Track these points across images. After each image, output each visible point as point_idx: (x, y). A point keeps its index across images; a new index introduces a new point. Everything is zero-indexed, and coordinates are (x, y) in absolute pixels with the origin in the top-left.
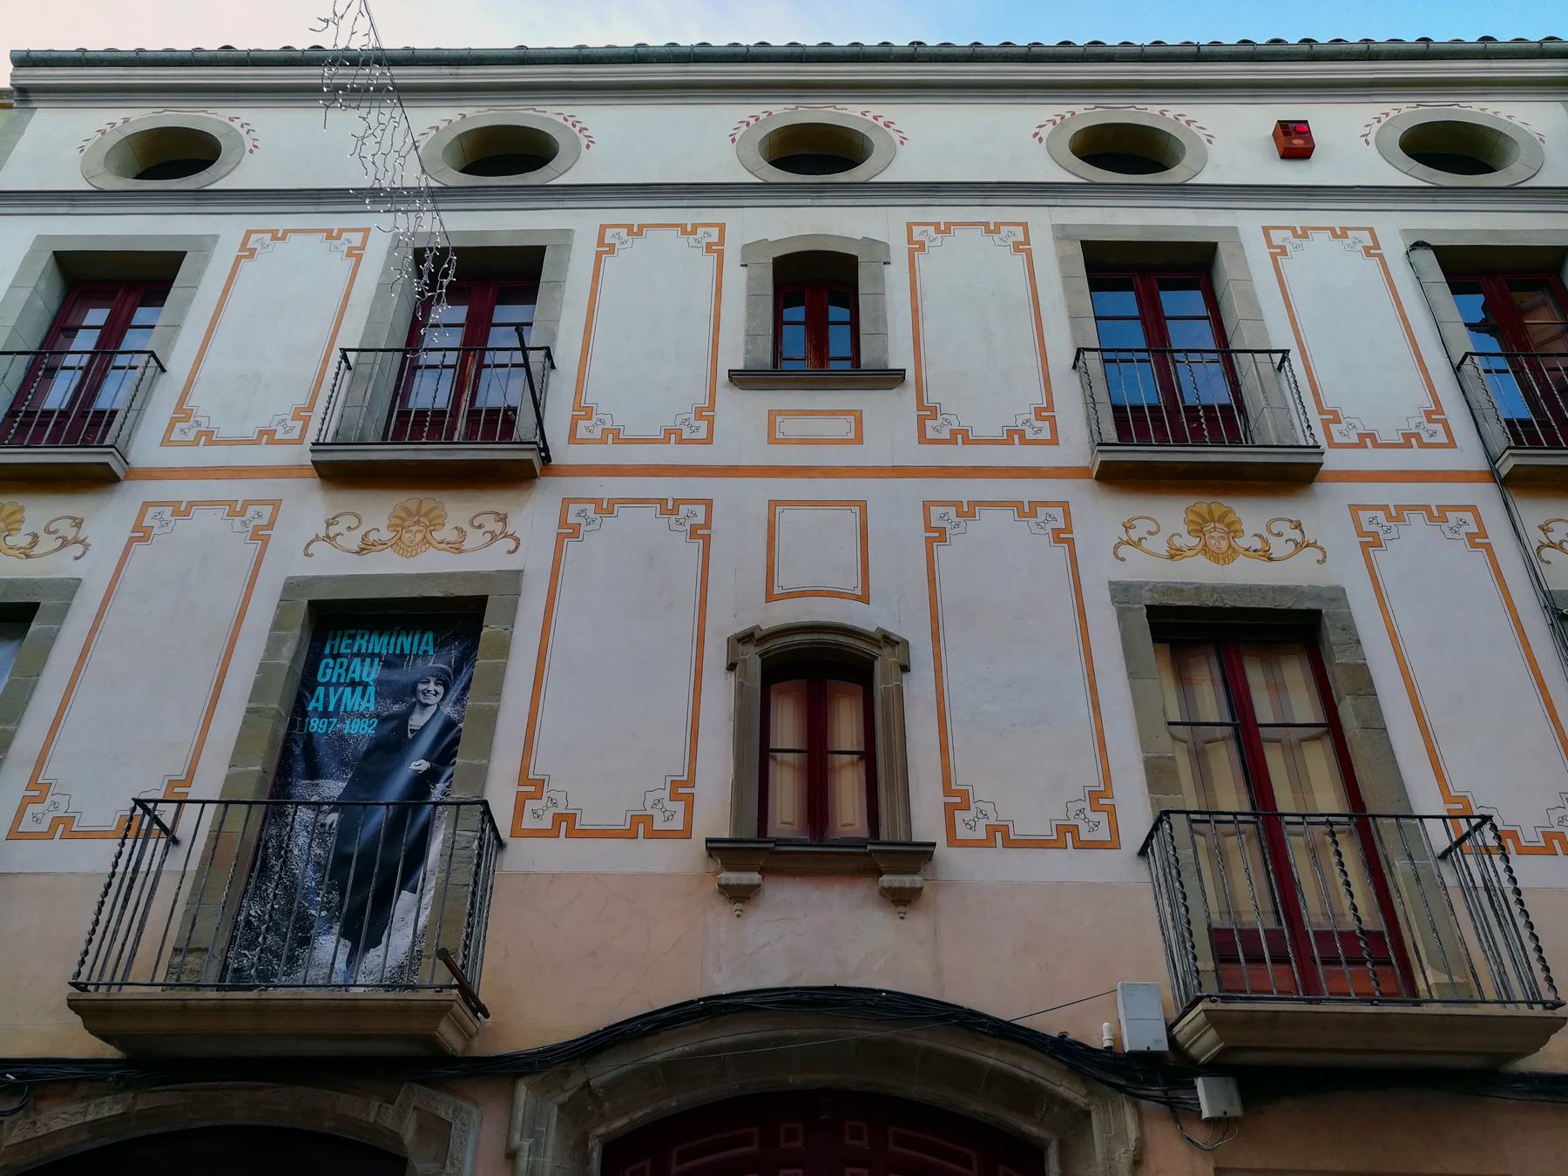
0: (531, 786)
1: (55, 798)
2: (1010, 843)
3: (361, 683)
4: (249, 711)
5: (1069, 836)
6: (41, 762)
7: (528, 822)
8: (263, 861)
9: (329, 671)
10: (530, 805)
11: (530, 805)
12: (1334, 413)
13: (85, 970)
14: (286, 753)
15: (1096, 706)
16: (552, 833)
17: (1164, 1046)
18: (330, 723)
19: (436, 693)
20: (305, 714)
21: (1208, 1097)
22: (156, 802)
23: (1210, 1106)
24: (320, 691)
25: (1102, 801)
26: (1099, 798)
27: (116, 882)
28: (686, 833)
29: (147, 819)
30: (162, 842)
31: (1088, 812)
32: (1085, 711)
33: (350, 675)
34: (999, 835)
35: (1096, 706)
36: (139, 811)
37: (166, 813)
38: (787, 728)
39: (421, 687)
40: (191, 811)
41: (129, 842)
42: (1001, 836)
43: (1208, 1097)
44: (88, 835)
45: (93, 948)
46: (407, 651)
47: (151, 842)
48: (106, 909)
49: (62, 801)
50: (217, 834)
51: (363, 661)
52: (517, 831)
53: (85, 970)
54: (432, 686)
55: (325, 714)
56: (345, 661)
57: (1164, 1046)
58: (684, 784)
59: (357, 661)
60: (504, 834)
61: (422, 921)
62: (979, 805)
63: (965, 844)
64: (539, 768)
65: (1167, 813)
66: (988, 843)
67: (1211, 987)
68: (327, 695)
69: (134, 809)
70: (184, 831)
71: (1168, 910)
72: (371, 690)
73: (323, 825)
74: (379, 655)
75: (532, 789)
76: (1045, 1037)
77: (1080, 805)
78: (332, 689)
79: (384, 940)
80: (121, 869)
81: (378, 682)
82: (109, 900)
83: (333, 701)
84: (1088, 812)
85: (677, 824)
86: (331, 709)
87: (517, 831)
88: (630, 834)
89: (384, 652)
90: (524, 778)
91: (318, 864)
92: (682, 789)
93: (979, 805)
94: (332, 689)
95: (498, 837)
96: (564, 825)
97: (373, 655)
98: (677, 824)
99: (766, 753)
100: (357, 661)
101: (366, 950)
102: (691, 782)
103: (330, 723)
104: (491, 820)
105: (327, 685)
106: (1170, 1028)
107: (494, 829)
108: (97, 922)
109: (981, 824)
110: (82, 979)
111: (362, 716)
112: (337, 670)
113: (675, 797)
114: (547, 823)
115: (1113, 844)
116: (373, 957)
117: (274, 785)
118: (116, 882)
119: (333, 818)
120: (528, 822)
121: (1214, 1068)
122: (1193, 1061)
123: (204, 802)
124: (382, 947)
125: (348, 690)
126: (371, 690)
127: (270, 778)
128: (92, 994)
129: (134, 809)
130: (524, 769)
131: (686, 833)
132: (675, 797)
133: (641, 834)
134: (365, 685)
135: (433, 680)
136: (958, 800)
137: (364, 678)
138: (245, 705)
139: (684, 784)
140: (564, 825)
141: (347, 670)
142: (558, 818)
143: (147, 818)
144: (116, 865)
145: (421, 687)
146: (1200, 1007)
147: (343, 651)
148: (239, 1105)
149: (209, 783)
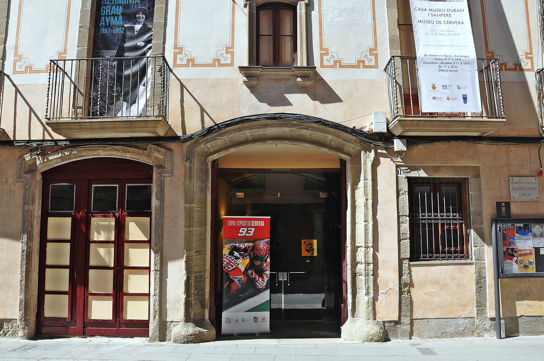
0: (178, 50)
1: (24, 60)
2: (341, 66)
3: (116, 15)
4: (80, 27)
5: (361, 64)
6: (16, 48)
7: (179, 62)
8: (92, 79)
9: (104, 11)
10: (179, 56)
11: (179, 56)
12: (327, 50)
13: (48, 114)
14: (95, 41)
15: (374, 18)
16: (187, 65)
17: (385, 131)
18: (108, 30)
19: (143, 18)
20: (99, 27)
21: (398, 145)
22: (57, 61)
23: (397, 148)
24: (103, 18)
25: (373, 52)
26: (373, 51)
27: (51, 86)
28: (232, 65)
29: (55, 66)
30: (61, 73)
31: (368, 56)
32: (370, 21)
33: (112, 12)
34: (338, 64)
35: (374, 18)
36: (52, 63)
37: (61, 64)
38: (266, 28)
39: (137, 16)
40: (68, 63)
41: (52, 74)
42: (338, 64)
43: (398, 145)
44: (38, 72)
45: (49, 107)
46: (131, 3)
47: (58, 73)
48: (50, 95)
49: (27, 61)
50: (78, 70)
51: (116, 7)
52: (175, 65)
53: (48, 114)
54: (141, 15)
55: (106, 27)
56: (110, 7)
57: (385, 131)
58: (230, 48)
59: (114, 7)
60: (171, 67)
61: (148, 95)
62: (332, 53)
63: (326, 67)
64: (180, 44)
65: (393, 57)
66: (334, 66)
67: (401, 113)
68: (105, 20)
69: (50, 63)
70: (68, 69)
71: (391, 88)
72: (120, 17)
73: (112, 65)
74: (121, 5)
75: (179, 51)
76: (348, 128)
77: (366, 54)
78: (106, 18)
79: (137, 101)
80: (51, 83)
81: (123, 14)
82: (50, 93)
83: (108, 21)
84: (368, 56)
85: (229, 62)
86: (107, 25)
87: (175, 65)
88: (213, 65)
89: (123, 3)
90: (176, 47)
91: (112, 78)
92: (230, 50)
93: (332, 53)
94: (106, 18)
95: (169, 68)
96: (190, 62)
97: (119, 5)
98: (229, 62)
99: (258, 35)
100: (114, 7)
101: (131, 105)
102: (232, 47)
103: (108, 30)
104: (166, 62)
105: (105, 16)
106: (388, 125)
107: (168, 65)
108: (48, 100)
109: (332, 60)
110: (48, 117)
111: (118, 27)
112: (107, 10)
113: (227, 52)
114: (185, 62)
115: (376, 66)
116: (134, 107)
117: (93, 53)
118: (51, 86)
119: (116, 63)
120: (179, 62)
121: (400, 137)
122: (394, 135)
123: (72, 60)
124: (137, 103)
125: (112, 18)
126: (120, 17)
127: (91, 50)
128: (52, 121)
129: (50, 63)
130: (175, 44)
131: (232, 65)
132: (227, 52)
133: (216, 65)
134: (118, 16)
135: (141, 13)
136: (325, 52)
137: (117, 13)
138: (79, 25)
139: (230, 48)
140: (190, 62)
141: (111, 10)
142: (188, 60)
143: (55, 66)
144: (49, 82)
145: (137, 16)
146: (397, 119)
147: (108, 3)
148: (102, 153)
149: (72, 54)
